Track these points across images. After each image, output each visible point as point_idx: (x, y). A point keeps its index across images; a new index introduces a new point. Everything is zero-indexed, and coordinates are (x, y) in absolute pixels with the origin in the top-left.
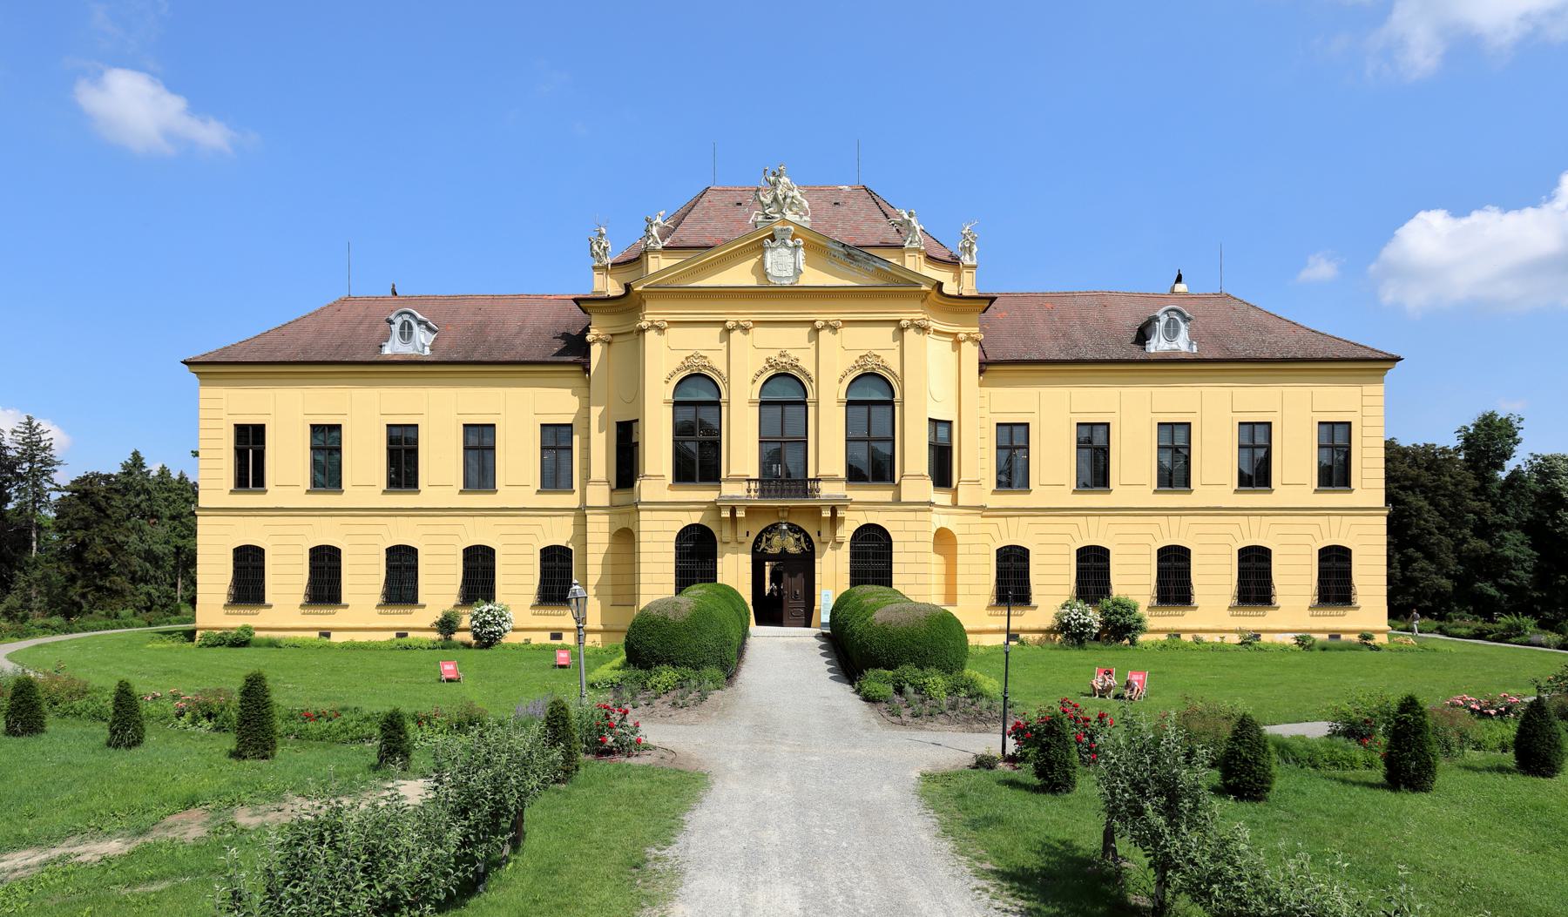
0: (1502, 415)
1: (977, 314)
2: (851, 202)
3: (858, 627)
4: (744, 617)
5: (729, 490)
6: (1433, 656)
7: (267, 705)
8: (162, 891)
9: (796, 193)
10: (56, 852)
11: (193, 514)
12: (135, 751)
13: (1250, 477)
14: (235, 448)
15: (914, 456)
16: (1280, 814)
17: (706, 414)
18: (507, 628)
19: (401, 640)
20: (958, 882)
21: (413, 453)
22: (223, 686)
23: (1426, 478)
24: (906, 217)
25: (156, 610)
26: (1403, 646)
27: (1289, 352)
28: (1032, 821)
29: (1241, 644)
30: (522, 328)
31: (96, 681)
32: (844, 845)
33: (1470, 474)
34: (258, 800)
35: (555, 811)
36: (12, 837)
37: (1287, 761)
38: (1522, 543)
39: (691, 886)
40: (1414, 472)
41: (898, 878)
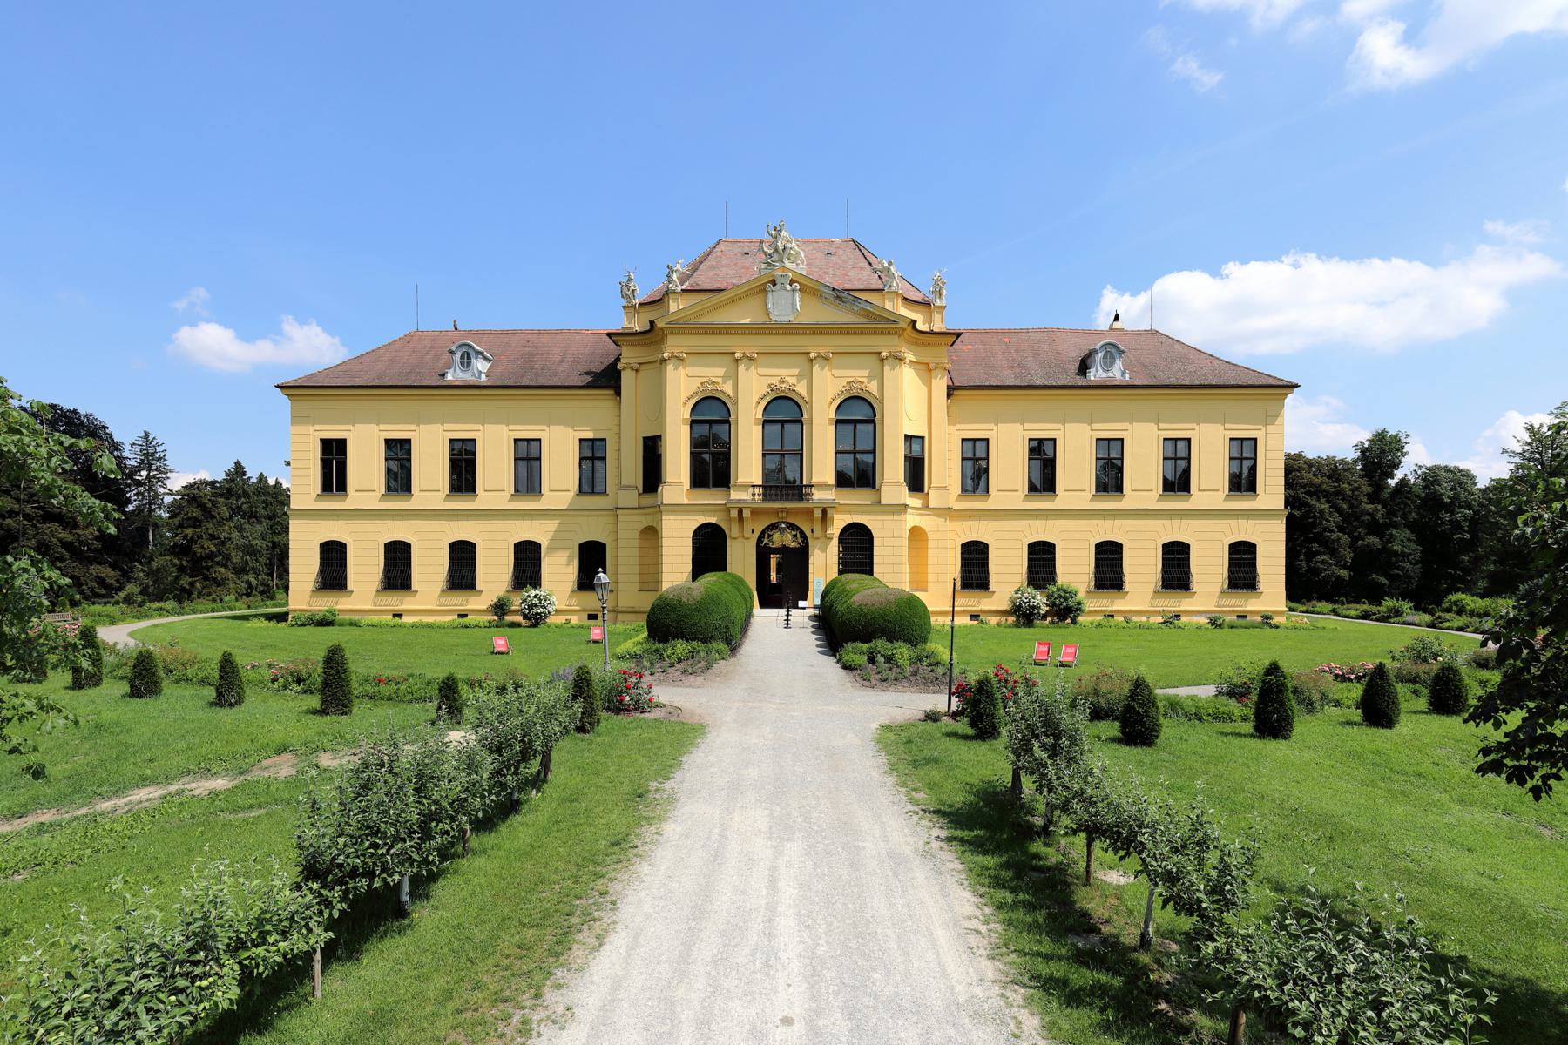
0: (1392, 431)
1: (946, 348)
2: (841, 252)
3: (840, 608)
4: (748, 599)
5: (735, 495)
6: (1321, 633)
7: (345, 671)
8: (259, 816)
9: (794, 245)
10: (173, 788)
11: (285, 514)
12: (237, 709)
13: (1173, 483)
14: (321, 459)
15: (893, 467)
16: (1164, 756)
17: (717, 428)
18: (551, 610)
19: (461, 620)
20: (895, 807)
21: (471, 464)
22: (311, 657)
23: (1328, 485)
24: (886, 265)
25: (255, 595)
26: (1298, 625)
27: (1205, 380)
28: (961, 761)
29: (1164, 623)
30: (563, 358)
31: (205, 654)
32: (809, 779)
33: (1364, 481)
34: (338, 747)
35: (580, 754)
36: (137, 777)
37: (1178, 715)
38: (1409, 539)
39: (682, 810)
40: (1316, 480)
41: (849, 804)
